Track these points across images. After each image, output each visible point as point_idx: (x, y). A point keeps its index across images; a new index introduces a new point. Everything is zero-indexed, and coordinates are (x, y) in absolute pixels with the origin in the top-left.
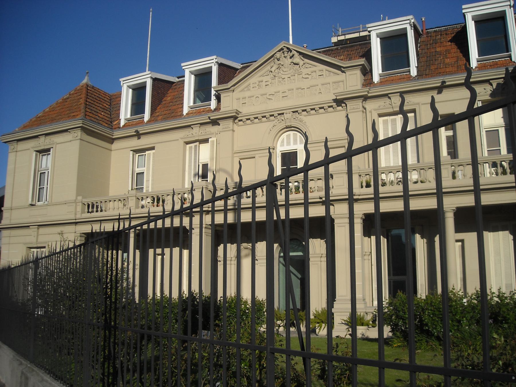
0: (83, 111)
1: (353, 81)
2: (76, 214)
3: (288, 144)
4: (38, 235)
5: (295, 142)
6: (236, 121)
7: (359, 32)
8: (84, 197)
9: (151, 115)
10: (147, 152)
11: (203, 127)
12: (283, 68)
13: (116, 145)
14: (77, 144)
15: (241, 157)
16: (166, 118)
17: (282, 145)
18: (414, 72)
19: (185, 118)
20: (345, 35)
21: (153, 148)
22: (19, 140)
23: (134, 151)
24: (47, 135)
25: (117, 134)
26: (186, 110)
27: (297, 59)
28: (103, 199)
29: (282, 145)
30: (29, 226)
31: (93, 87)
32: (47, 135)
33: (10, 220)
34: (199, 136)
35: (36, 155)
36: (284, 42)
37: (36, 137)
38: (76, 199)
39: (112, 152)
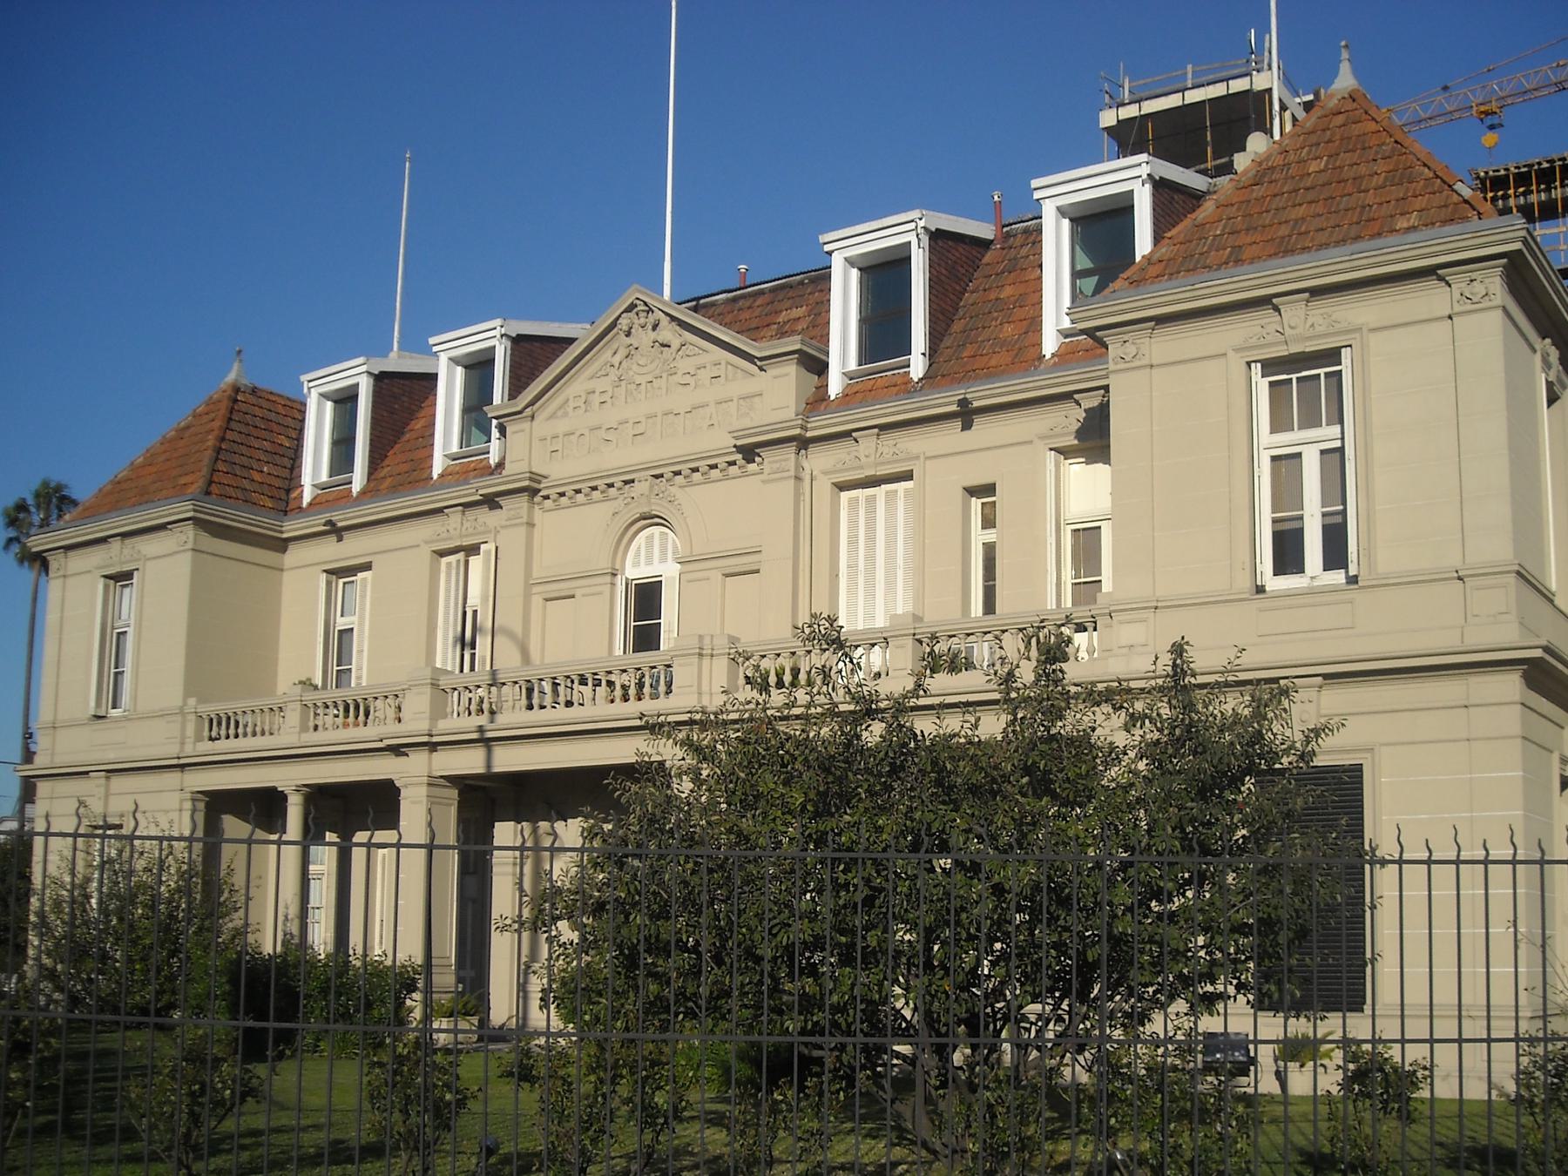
0: (205, 471)
1: (776, 395)
2: (183, 743)
3: (649, 562)
4: (107, 796)
5: (663, 560)
6: (537, 499)
7: (1183, 91)
8: (201, 701)
9: (370, 474)
10: (360, 575)
11: (471, 514)
12: (637, 357)
13: (294, 555)
14: (184, 562)
15: (728, 571)
16: (396, 489)
17: (636, 564)
18: (917, 366)
19: (436, 487)
20: (1139, 101)
21: (367, 567)
22: (68, 548)
23: (1269, 366)
24: (125, 535)
25: (292, 527)
26: (438, 467)
27: (668, 332)
28: (265, 702)
29: (636, 564)
30: (87, 773)
31: (254, 391)
32: (125, 535)
33: (53, 754)
34: (461, 536)
35: (106, 587)
36: (635, 286)
37: (104, 540)
38: (185, 703)
39: (285, 574)
